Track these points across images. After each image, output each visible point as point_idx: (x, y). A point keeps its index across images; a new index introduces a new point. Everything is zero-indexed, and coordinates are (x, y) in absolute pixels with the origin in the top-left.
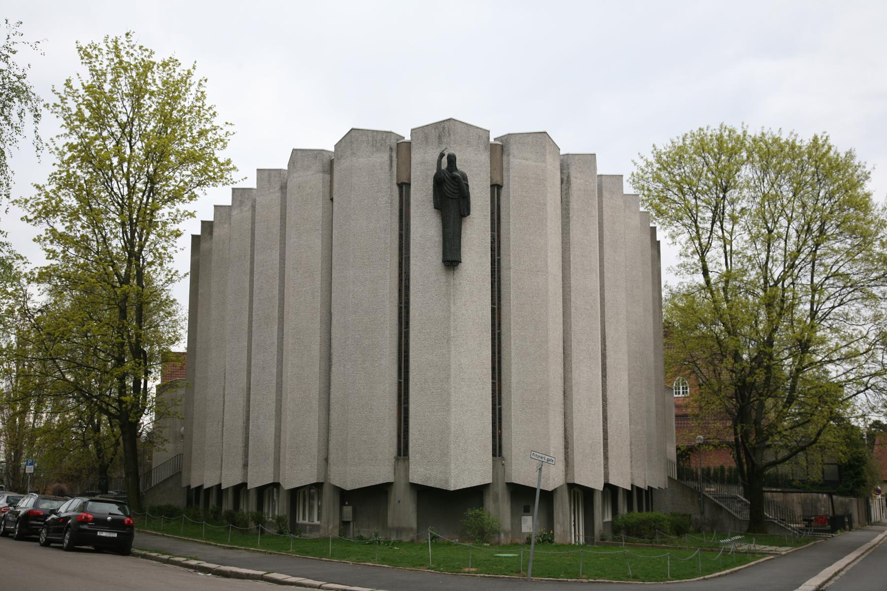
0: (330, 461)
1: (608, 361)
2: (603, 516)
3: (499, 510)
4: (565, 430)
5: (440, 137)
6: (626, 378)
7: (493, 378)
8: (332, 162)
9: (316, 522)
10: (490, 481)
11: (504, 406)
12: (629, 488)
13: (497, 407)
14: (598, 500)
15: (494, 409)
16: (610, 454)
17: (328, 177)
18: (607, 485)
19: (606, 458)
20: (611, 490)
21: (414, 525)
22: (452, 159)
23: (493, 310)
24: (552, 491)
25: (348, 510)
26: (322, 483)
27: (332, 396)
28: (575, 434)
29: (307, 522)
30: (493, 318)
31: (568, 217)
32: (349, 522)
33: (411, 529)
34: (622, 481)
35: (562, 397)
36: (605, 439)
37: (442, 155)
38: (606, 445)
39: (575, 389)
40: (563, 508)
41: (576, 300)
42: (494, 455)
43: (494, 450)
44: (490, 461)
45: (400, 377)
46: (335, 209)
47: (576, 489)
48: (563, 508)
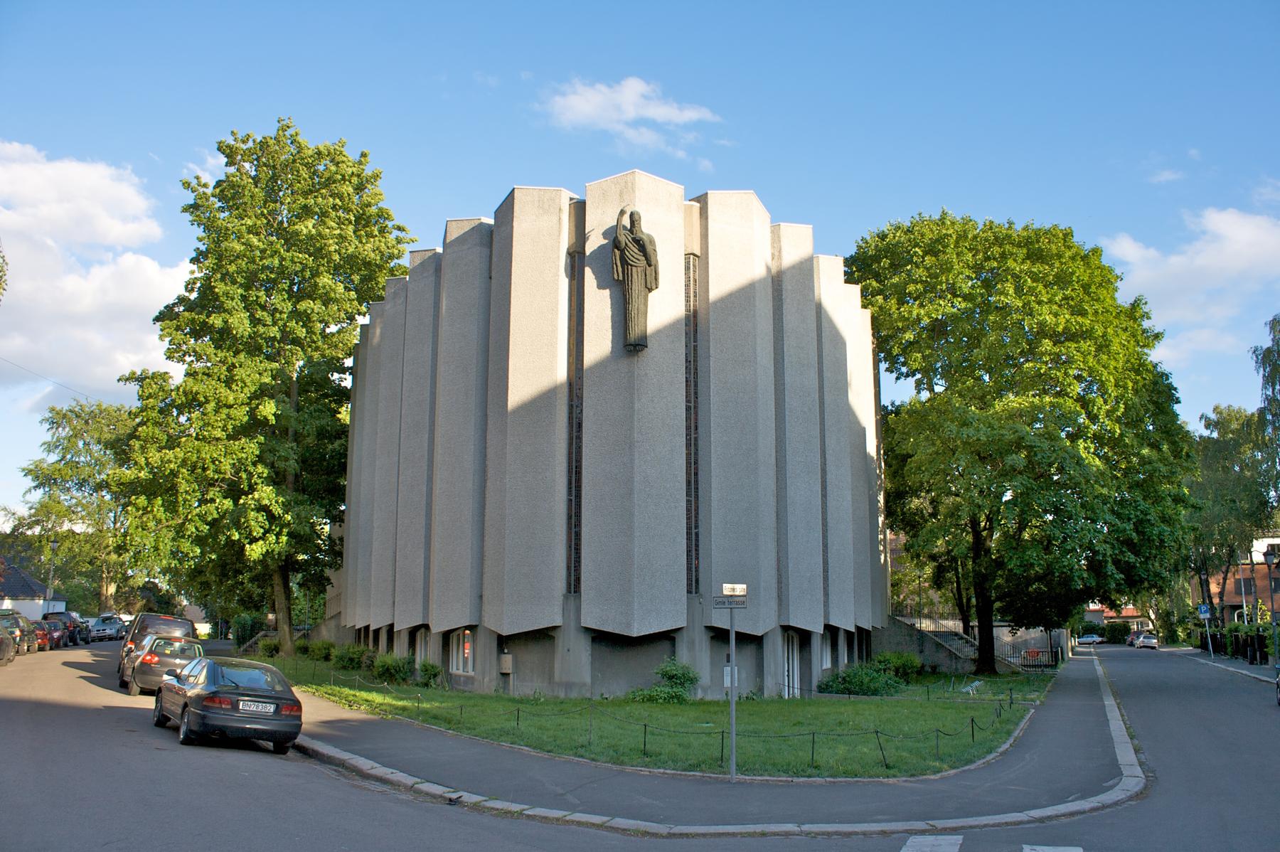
0: (485, 598)
1: (829, 476)
2: (822, 661)
3: (695, 655)
4: (778, 560)
5: (621, 194)
6: (849, 498)
7: (688, 494)
8: (492, 232)
9: (471, 673)
10: (684, 625)
11: (701, 530)
12: (853, 630)
13: (694, 531)
14: (816, 643)
15: (689, 533)
16: (831, 589)
17: (486, 251)
18: (828, 628)
19: (826, 594)
20: (831, 632)
21: (588, 680)
22: (634, 218)
23: (688, 409)
24: (762, 637)
25: (508, 661)
26: (476, 626)
27: (487, 518)
28: (790, 565)
29: (460, 672)
30: (688, 419)
31: (781, 300)
32: (508, 674)
33: (585, 684)
34: (846, 623)
35: (774, 519)
36: (826, 571)
37: (622, 213)
38: (826, 579)
39: (790, 509)
40: (776, 649)
41: (791, 401)
42: (689, 592)
43: (689, 585)
44: (685, 598)
45: (570, 493)
46: (493, 288)
47: (791, 633)
48: (776, 649)
